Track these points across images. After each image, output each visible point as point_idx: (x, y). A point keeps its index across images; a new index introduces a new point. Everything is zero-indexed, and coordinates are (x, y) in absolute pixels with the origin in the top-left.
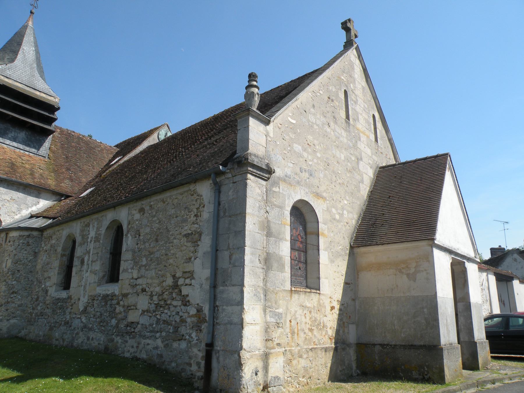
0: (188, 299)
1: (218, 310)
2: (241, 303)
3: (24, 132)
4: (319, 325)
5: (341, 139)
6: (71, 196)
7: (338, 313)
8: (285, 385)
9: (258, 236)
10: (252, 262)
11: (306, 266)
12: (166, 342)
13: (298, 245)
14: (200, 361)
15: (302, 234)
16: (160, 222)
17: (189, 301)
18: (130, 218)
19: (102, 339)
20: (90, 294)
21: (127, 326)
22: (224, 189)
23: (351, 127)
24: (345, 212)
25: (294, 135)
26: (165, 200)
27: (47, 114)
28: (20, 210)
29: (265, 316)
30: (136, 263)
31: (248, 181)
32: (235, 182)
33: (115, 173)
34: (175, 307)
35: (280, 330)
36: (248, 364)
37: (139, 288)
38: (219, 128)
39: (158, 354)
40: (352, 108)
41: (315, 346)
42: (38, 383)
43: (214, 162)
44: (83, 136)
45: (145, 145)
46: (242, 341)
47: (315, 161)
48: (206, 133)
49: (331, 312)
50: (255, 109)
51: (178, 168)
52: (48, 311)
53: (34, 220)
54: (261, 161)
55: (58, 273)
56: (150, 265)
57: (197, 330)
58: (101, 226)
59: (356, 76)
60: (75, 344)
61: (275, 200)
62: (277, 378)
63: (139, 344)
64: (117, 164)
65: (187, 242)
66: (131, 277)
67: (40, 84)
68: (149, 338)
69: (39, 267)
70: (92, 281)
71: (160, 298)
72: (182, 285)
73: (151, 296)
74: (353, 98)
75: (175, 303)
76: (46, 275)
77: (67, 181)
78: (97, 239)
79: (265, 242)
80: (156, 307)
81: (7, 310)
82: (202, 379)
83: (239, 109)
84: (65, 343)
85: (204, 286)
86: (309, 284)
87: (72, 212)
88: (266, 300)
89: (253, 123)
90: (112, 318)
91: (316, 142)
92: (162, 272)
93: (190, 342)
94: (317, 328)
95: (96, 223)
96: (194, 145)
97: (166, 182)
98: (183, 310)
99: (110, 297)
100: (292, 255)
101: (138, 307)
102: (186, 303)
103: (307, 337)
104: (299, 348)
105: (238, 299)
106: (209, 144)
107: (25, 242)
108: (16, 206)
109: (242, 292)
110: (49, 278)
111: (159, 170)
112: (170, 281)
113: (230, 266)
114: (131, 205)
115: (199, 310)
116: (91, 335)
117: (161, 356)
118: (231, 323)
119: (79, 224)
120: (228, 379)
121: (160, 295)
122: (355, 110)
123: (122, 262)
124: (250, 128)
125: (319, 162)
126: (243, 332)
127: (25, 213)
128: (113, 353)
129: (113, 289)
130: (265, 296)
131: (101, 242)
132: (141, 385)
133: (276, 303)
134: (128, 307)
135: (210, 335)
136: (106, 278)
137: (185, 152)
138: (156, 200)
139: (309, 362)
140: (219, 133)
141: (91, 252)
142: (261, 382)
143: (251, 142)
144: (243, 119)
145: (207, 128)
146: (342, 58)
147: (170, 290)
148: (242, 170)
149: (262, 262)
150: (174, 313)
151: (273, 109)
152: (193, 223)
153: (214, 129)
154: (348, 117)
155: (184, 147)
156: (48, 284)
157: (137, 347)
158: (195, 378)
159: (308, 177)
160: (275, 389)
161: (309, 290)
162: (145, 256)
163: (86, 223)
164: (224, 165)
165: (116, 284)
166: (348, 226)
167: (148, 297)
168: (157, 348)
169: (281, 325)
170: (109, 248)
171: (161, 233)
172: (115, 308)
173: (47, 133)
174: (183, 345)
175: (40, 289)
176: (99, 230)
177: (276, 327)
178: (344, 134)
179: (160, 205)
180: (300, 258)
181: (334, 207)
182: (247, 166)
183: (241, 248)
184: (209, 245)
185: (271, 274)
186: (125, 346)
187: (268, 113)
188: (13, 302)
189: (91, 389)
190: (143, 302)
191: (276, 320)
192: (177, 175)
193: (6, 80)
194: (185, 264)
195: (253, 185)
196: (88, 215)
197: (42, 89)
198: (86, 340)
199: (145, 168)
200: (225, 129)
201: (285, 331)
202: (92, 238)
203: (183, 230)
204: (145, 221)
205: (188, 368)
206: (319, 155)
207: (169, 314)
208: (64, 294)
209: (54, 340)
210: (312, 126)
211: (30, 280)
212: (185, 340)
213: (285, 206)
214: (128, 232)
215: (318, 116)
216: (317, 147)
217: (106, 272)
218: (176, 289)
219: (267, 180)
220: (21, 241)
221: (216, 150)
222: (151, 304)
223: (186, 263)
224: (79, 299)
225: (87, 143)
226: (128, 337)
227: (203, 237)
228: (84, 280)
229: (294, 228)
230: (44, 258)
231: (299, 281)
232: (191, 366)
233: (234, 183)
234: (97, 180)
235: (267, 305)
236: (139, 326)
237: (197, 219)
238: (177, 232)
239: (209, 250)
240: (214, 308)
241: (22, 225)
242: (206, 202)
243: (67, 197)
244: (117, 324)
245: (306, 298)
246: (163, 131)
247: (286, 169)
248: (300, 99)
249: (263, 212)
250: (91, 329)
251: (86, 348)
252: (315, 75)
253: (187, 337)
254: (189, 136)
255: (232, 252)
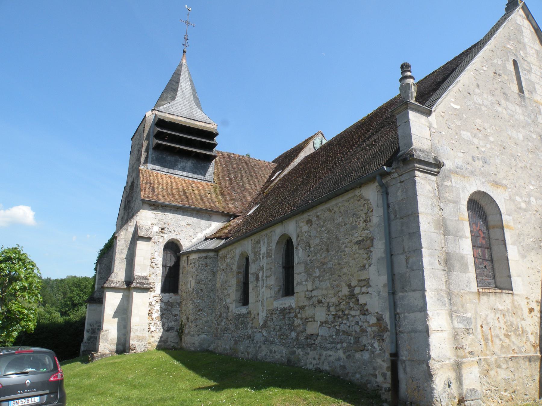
0: (366, 307)
1: (399, 317)
2: (424, 309)
3: (190, 161)
4: (517, 329)
5: (516, 116)
6: (239, 216)
7: (539, 315)
8: (485, 399)
9: (434, 236)
10: (431, 264)
11: (492, 264)
12: (348, 353)
13: (480, 241)
14: (386, 372)
15: (484, 229)
16: (329, 232)
17: (367, 310)
18: (298, 230)
19: (284, 351)
20: (268, 309)
21: (307, 338)
22: (391, 190)
23: (527, 101)
24: (532, 199)
25: (460, 122)
26: (331, 209)
27: (208, 141)
28: (196, 234)
29: (452, 322)
30: (309, 275)
31: (417, 179)
32: (403, 182)
33: (277, 188)
34: (354, 316)
35: (471, 337)
36: (439, 374)
37: (315, 300)
38: (376, 128)
39: (341, 366)
40: (526, 79)
41: (516, 355)
42: (233, 393)
43: (376, 163)
44: (242, 157)
45: (302, 156)
46: (429, 349)
47: (488, 146)
48: (363, 135)
49: (530, 315)
50: (413, 101)
51: (340, 175)
52: (232, 327)
53: (209, 242)
54: (427, 156)
55: (236, 290)
56: (324, 275)
57: (379, 340)
58: (271, 242)
59: (526, 40)
60: (259, 357)
61: (448, 195)
62: (473, 391)
63: (320, 355)
64: (278, 179)
65: (359, 249)
66: (306, 289)
67: (199, 114)
68: (330, 349)
69: (218, 285)
70: (269, 296)
71: (338, 308)
72: (359, 294)
73: (328, 307)
74: (525, 66)
75: (353, 313)
76: (225, 292)
77: (233, 202)
78: (269, 255)
79: (443, 241)
80: (334, 318)
81: (197, 326)
82: (389, 391)
83: (394, 104)
84: (250, 356)
85: (381, 293)
86: (498, 284)
87: (243, 231)
88: (451, 304)
89: (413, 115)
90: (292, 331)
91: (486, 125)
92: (337, 282)
93: (373, 352)
94: (515, 334)
95: (266, 240)
96: (352, 149)
97: (330, 191)
98: (362, 320)
99: (287, 311)
100: (475, 253)
101: (316, 319)
102: (365, 312)
103: (504, 344)
104: (496, 357)
105: (421, 305)
106: (368, 146)
107: (204, 263)
108: (192, 230)
109: (424, 297)
110: (229, 295)
111: (321, 180)
112: (345, 291)
113: (408, 270)
114: (298, 218)
115: (380, 319)
116: (274, 348)
117: (344, 367)
118: (414, 331)
119: (250, 242)
120: (418, 391)
121: (336, 306)
122: (530, 81)
123: (295, 275)
124: (411, 122)
125: (493, 146)
126: (430, 340)
127: (201, 236)
128: (296, 365)
129: (289, 302)
130: (450, 299)
131: (273, 257)
132: (328, 397)
133: (462, 307)
134: (306, 319)
135: (394, 345)
136: (281, 292)
137: (344, 157)
138: (323, 210)
139: (510, 373)
140: (376, 132)
141: (265, 268)
142: (456, 395)
143: (413, 137)
144: (401, 114)
145: (363, 130)
146: (505, 23)
147: (347, 300)
148: (408, 167)
149: (442, 263)
150: (353, 323)
151: (433, 98)
152: (364, 229)
153: (371, 129)
154: (521, 90)
155: (343, 153)
156: (228, 301)
157: (319, 359)
158: (381, 390)
159: (483, 165)
160: (472, 403)
161: (499, 291)
162: (317, 267)
163: (256, 240)
164: (389, 164)
165: (292, 297)
166: (538, 214)
167: (325, 308)
168: (339, 359)
169: (471, 331)
170: (281, 263)
171: (332, 242)
172: (294, 321)
173: (210, 158)
174: (366, 355)
175: (222, 306)
176: (270, 246)
177: (466, 333)
178: (519, 110)
179: (327, 214)
180: (484, 255)
181: (517, 195)
182: (414, 163)
183: (418, 251)
184: (382, 250)
185: (454, 275)
186: (307, 358)
187: (428, 103)
188: (201, 319)
189: (280, 399)
190: (320, 314)
191: (465, 325)
192: (341, 182)
193: (171, 116)
194: (360, 272)
195: (423, 182)
196: (257, 232)
197: (201, 119)
198: (269, 353)
199: (306, 179)
200: (382, 127)
201: (476, 338)
202: (264, 254)
203: (354, 237)
204: (314, 233)
205: (373, 379)
206: (491, 139)
207: (348, 324)
208: (244, 310)
209: (240, 353)
210: (479, 109)
211: (212, 298)
212: (368, 350)
213: (460, 201)
214: (298, 245)
215: (485, 96)
216: (489, 131)
217: (281, 286)
218: (353, 298)
219: (436, 174)
220: (200, 263)
221: (377, 150)
222: (329, 315)
223: (361, 270)
224: (258, 314)
225: (246, 163)
226: (309, 349)
227: (375, 243)
228: (261, 295)
229: (473, 224)
230: (222, 277)
231: (486, 281)
232: (376, 378)
233: (401, 182)
234: (260, 197)
235: (453, 309)
236: (319, 338)
237: (366, 225)
238: (348, 240)
239: (383, 255)
240: (395, 315)
241: (200, 248)
242: (374, 206)
243: (235, 216)
244: (297, 337)
245: (497, 299)
246: (317, 139)
247: (456, 160)
248: (461, 81)
249: (436, 209)
250: (272, 343)
251: (269, 360)
252: (474, 50)
253: (370, 347)
254: (345, 140)
255: (408, 255)
